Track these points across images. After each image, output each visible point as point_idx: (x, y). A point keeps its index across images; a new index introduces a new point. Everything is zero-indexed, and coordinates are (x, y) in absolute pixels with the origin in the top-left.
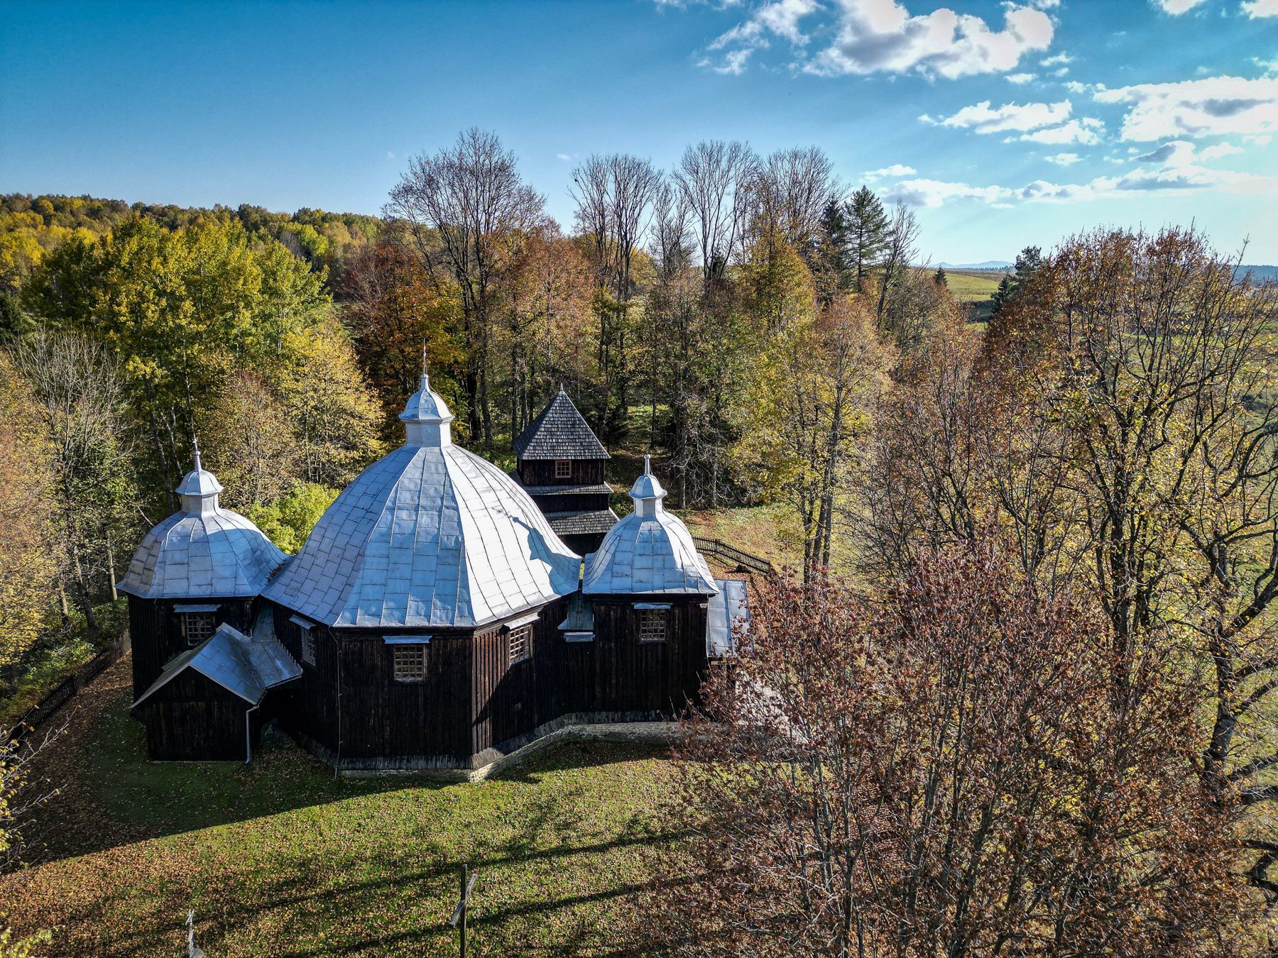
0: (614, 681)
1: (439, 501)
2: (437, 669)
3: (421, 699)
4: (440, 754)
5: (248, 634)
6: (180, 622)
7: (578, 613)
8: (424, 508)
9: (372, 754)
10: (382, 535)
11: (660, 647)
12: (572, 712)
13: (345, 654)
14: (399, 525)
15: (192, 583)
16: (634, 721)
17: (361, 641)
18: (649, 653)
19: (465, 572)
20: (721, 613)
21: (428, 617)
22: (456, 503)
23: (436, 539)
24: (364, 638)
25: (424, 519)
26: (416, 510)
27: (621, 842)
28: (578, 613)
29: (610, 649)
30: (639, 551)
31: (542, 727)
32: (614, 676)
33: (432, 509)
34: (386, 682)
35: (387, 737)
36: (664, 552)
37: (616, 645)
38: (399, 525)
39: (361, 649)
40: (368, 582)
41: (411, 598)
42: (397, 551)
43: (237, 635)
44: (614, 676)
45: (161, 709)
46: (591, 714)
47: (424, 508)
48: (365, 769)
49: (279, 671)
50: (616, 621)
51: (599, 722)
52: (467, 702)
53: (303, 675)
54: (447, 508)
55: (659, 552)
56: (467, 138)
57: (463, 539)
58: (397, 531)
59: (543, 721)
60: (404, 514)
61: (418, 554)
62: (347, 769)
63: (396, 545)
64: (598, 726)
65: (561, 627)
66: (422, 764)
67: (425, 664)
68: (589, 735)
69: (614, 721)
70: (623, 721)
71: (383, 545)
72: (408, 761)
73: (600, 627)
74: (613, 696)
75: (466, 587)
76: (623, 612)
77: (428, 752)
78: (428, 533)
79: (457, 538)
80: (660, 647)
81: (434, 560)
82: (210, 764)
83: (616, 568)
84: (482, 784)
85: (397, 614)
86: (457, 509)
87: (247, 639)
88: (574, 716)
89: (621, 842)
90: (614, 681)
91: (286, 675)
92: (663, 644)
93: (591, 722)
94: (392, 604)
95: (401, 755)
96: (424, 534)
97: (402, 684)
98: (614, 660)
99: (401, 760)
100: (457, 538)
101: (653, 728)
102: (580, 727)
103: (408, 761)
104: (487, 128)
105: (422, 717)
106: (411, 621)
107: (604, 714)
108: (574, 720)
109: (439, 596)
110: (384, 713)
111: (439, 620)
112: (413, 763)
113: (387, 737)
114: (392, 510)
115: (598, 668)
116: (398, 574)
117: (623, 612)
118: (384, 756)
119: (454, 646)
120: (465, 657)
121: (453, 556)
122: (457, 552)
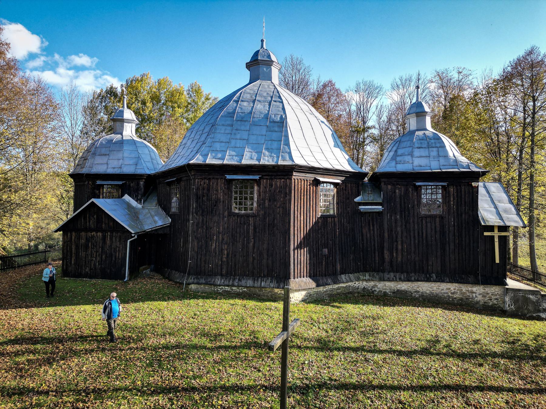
0: (400, 247)
1: (270, 99)
2: (264, 203)
3: (251, 228)
4: (264, 276)
5: (140, 203)
6: (100, 192)
7: (369, 194)
8: (259, 101)
9: (212, 274)
10: (229, 113)
11: (438, 219)
12: (366, 271)
13: (198, 189)
14: (241, 109)
15: (109, 166)
16: (418, 281)
17: (210, 179)
18: (429, 225)
19: (287, 137)
20: (486, 200)
21: (259, 160)
22: (281, 99)
23: (267, 116)
24: (211, 177)
25: (259, 106)
26: (254, 101)
27: (425, 352)
28: (369, 194)
29: (396, 220)
30: (416, 145)
31: (343, 276)
32: (399, 242)
33: (264, 101)
34: (226, 213)
35: (224, 259)
36: (438, 145)
37: (401, 217)
38: (241, 109)
39: (209, 185)
40: (218, 140)
41: (247, 149)
42: (239, 123)
43: (134, 203)
44: (399, 242)
45: (73, 238)
46: (381, 274)
47: (259, 101)
48: (206, 284)
49: (155, 222)
50: (400, 197)
51: (389, 280)
52: (286, 233)
53: (171, 224)
54: (275, 101)
55: (434, 145)
56: (288, 59)
57: (286, 116)
58: (240, 111)
59: (344, 272)
60: (245, 104)
61: (255, 124)
62: (193, 283)
63: (238, 119)
64: (388, 284)
65: (357, 199)
66: (250, 283)
67: (256, 199)
68: (380, 291)
69: (401, 280)
70: (409, 280)
71: (229, 119)
72: (239, 280)
73: (387, 202)
74: (399, 259)
75: (288, 144)
76: (407, 190)
77: (255, 275)
78: (261, 113)
79: (282, 116)
80: (438, 219)
81: (264, 129)
82: (99, 281)
83: (398, 159)
84: (297, 304)
85: (236, 158)
86: (282, 102)
87: (140, 206)
88: (367, 275)
89: (425, 352)
90: (400, 247)
91: (160, 223)
92: (441, 217)
93: (382, 279)
94: (234, 153)
95: (234, 276)
96: (259, 113)
97: (238, 215)
98: (399, 229)
99: (234, 279)
100: (282, 116)
101: (435, 289)
102: (372, 283)
103: (239, 280)
104: (297, 55)
105: (251, 244)
106: (246, 161)
107: (392, 275)
108: (367, 277)
109: (267, 149)
110: (223, 239)
111: (267, 160)
112: (243, 282)
113: (224, 259)
114: (237, 102)
115: (386, 235)
116: (238, 136)
117: (407, 190)
118: (222, 275)
119: (278, 184)
120: (286, 193)
121: (279, 126)
122: (282, 123)
